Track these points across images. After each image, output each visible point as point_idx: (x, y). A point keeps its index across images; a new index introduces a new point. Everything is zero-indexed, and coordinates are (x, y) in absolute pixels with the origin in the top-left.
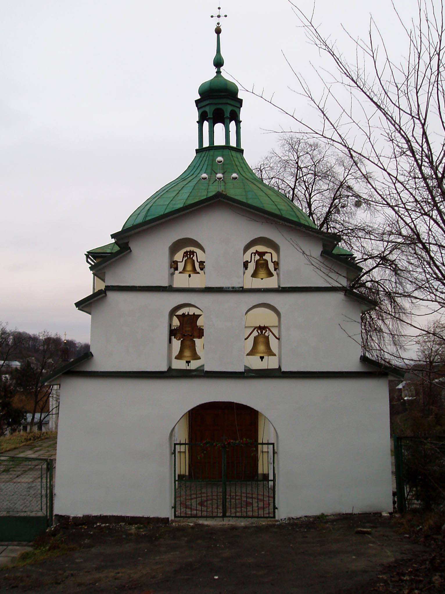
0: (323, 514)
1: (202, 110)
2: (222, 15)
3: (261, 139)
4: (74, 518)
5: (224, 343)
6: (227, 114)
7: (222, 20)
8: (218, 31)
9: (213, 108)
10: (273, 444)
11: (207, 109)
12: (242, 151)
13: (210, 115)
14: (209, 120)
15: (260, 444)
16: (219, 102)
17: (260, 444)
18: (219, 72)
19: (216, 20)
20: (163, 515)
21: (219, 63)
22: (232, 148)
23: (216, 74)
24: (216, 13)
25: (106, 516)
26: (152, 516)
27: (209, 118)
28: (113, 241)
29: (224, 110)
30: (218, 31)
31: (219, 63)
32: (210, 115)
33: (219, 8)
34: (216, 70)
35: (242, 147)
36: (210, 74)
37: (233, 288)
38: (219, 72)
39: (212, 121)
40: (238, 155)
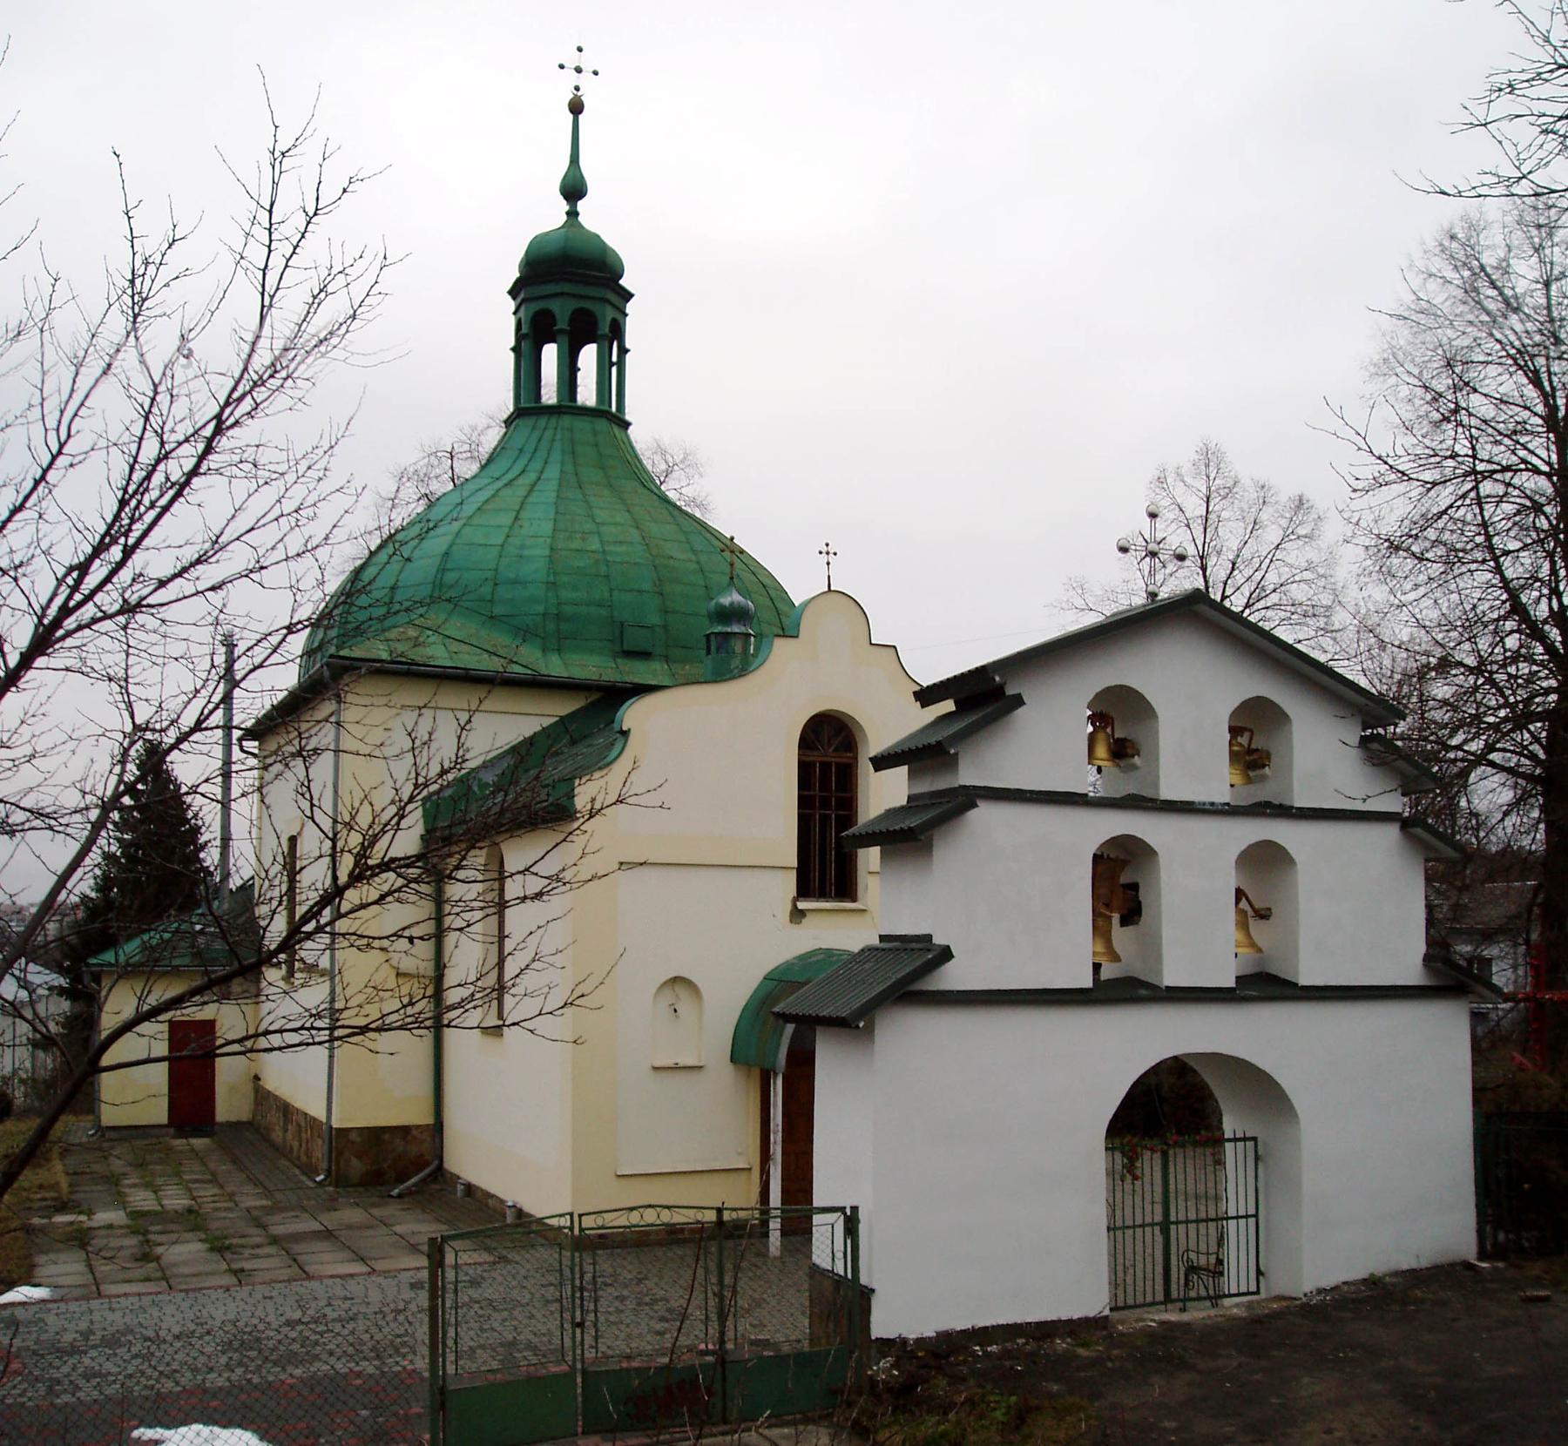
0: (1372, 1275)
1: (536, 306)
2: (587, 68)
3: (677, 394)
4: (918, 1340)
5: (1194, 931)
6: (605, 328)
7: (585, 80)
8: (576, 108)
9: (573, 305)
10: (1255, 1139)
11: (555, 306)
12: (626, 425)
13: (562, 323)
14: (559, 338)
15: (1229, 1140)
16: (570, 293)
17: (1229, 1140)
18: (573, 214)
19: (571, 79)
20: (1091, 1313)
21: (573, 190)
22: (585, 411)
23: (565, 218)
24: (572, 60)
25: (986, 1328)
26: (1075, 1317)
27: (561, 331)
28: (1010, 691)
29: (599, 314)
30: (576, 108)
31: (573, 190)
32: (562, 323)
33: (580, 50)
34: (567, 208)
35: (628, 418)
36: (553, 215)
37: (1212, 804)
38: (573, 214)
39: (565, 339)
40: (616, 430)
